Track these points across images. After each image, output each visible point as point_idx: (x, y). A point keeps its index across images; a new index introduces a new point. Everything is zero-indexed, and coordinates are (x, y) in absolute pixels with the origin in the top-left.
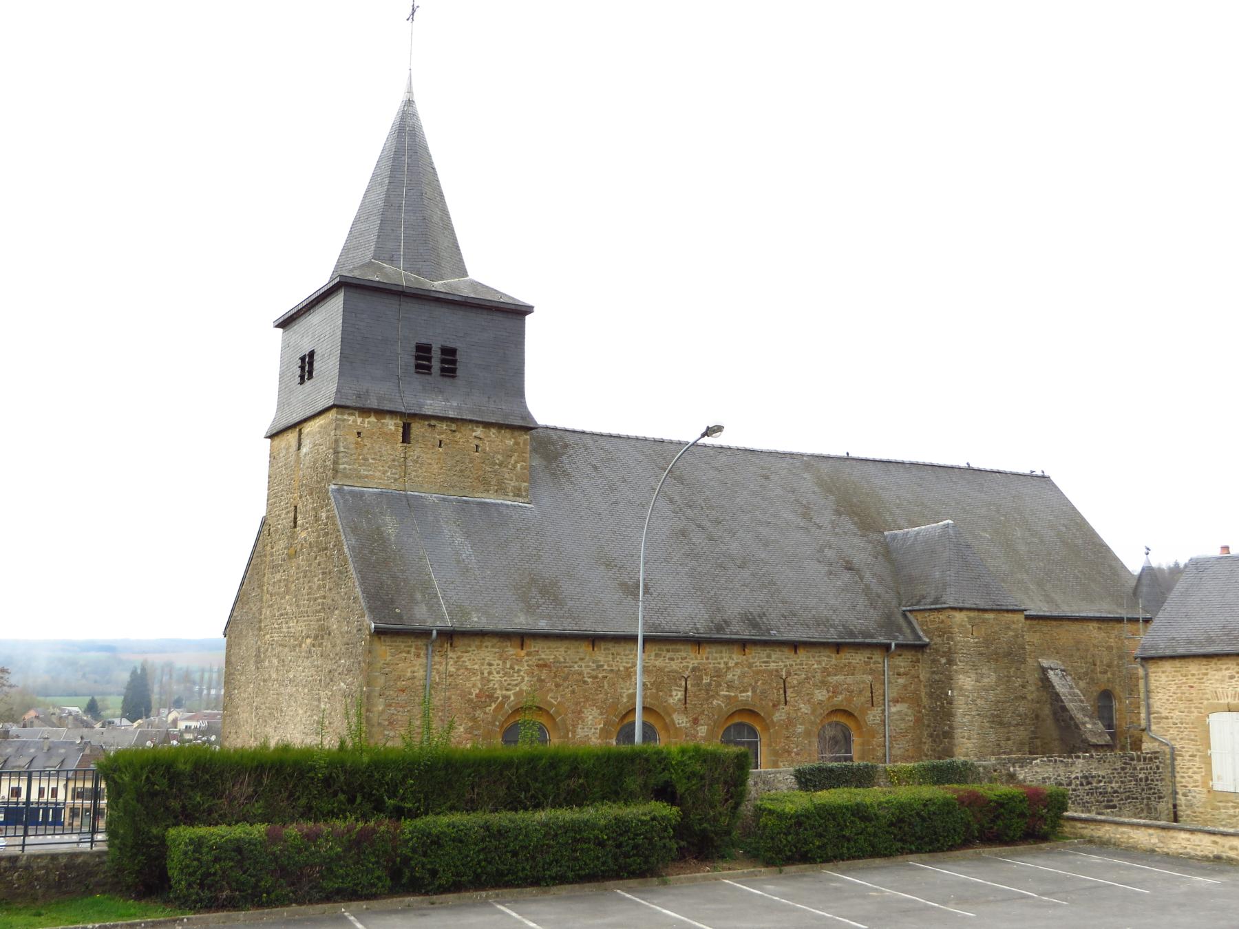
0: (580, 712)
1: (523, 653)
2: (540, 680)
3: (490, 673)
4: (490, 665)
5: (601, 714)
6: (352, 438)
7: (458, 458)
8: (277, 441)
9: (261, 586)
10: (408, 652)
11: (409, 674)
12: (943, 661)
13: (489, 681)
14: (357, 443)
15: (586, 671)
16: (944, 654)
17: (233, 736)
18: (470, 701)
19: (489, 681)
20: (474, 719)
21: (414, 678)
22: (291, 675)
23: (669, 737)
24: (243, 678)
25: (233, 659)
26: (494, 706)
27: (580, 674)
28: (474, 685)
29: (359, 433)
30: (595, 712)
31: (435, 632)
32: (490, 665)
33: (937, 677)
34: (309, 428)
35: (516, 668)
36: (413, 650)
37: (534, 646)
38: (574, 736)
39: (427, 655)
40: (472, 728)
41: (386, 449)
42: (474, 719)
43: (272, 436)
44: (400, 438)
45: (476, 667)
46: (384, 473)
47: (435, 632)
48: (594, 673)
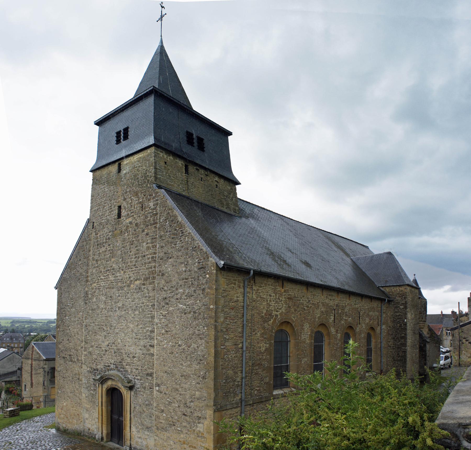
0: (303, 326)
1: (283, 290)
2: (289, 307)
3: (270, 301)
4: (270, 296)
5: (310, 327)
6: (162, 164)
7: (210, 188)
8: (98, 173)
9: (87, 258)
10: (235, 284)
11: (235, 298)
12: (402, 307)
13: (270, 305)
14: (165, 167)
15: (305, 303)
16: (403, 304)
17: (65, 342)
18: (262, 317)
19: (270, 305)
20: (264, 328)
21: (238, 301)
22: (120, 304)
23: (330, 339)
24: (73, 310)
25: (64, 300)
26: (272, 320)
27: (303, 304)
28: (264, 308)
29: (166, 163)
30: (308, 325)
31: (252, 272)
32: (270, 296)
33: (398, 314)
34: (125, 162)
35: (281, 298)
36: (237, 283)
37: (288, 286)
38: (301, 338)
39: (244, 287)
40: (263, 333)
41: (179, 174)
42: (264, 328)
43: (91, 171)
44: (184, 170)
45: (265, 296)
46: (179, 185)
47: (252, 272)
48: (307, 304)
